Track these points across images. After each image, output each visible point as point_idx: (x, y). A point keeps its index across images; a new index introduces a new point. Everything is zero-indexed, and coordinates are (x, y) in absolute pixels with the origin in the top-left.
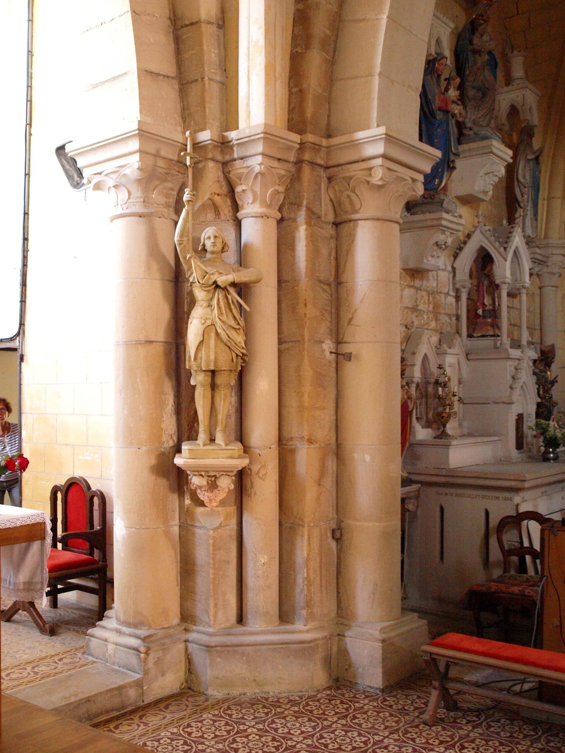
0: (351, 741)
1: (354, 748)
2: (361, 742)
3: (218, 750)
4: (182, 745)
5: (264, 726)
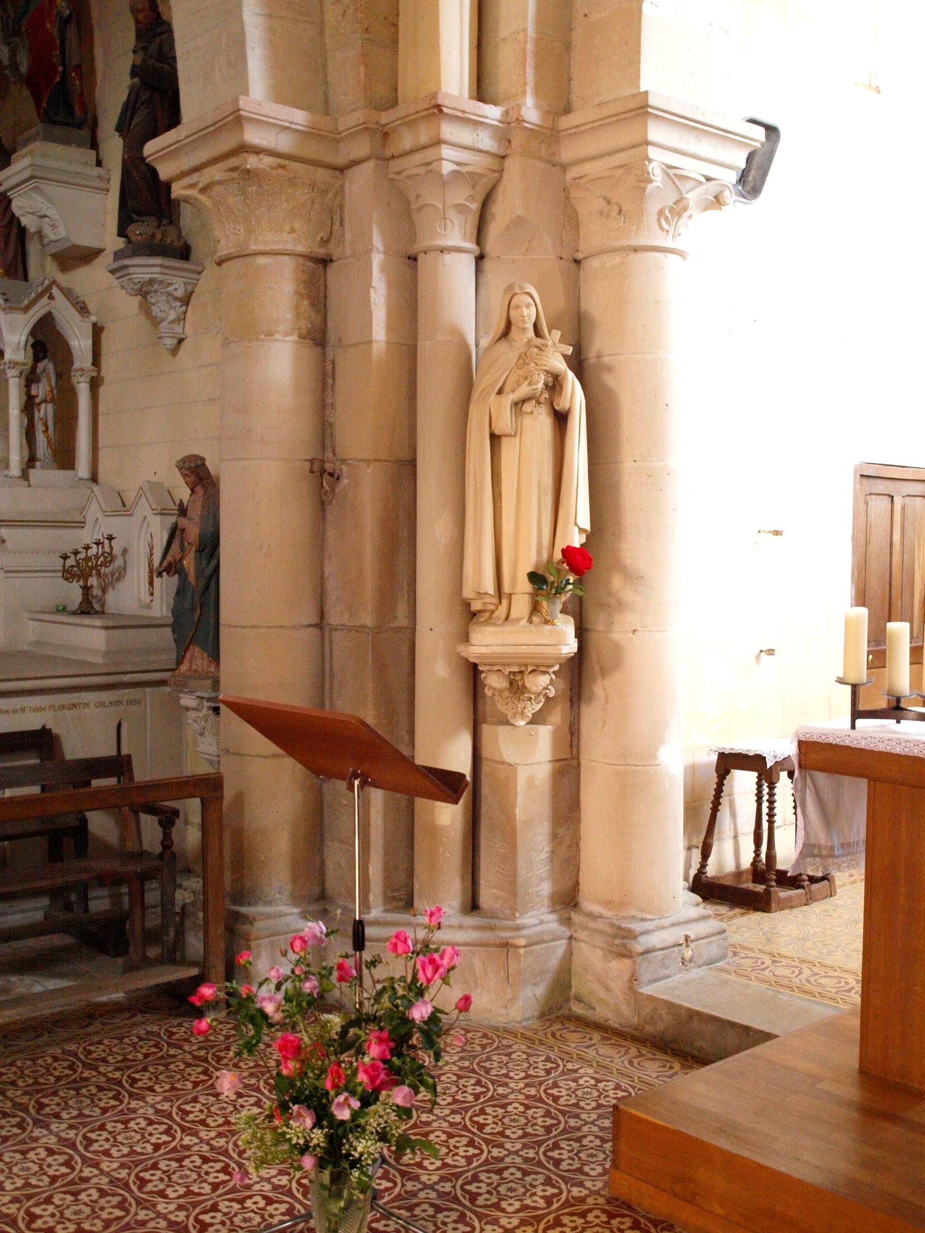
0: (62, 1213)
1: (108, 1223)
2: (41, 1217)
3: (171, 1224)
4: (487, 1125)
5: (566, 1122)
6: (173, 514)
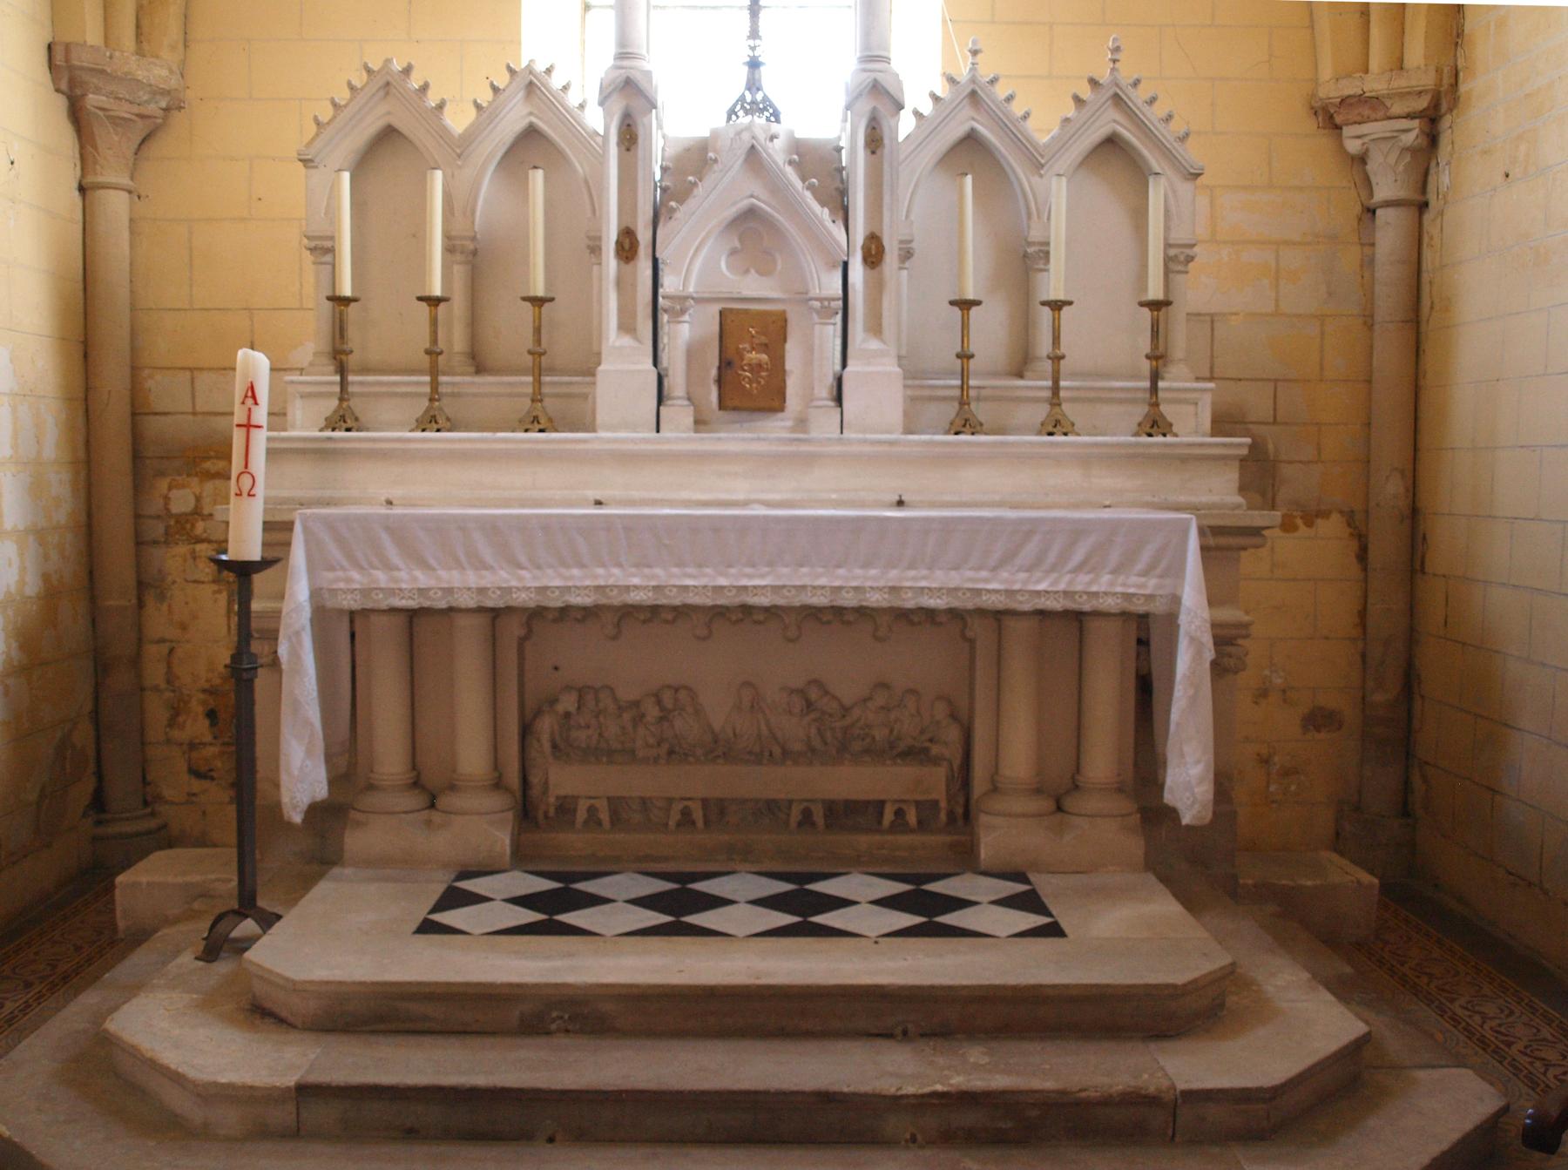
6: (1036, 400)
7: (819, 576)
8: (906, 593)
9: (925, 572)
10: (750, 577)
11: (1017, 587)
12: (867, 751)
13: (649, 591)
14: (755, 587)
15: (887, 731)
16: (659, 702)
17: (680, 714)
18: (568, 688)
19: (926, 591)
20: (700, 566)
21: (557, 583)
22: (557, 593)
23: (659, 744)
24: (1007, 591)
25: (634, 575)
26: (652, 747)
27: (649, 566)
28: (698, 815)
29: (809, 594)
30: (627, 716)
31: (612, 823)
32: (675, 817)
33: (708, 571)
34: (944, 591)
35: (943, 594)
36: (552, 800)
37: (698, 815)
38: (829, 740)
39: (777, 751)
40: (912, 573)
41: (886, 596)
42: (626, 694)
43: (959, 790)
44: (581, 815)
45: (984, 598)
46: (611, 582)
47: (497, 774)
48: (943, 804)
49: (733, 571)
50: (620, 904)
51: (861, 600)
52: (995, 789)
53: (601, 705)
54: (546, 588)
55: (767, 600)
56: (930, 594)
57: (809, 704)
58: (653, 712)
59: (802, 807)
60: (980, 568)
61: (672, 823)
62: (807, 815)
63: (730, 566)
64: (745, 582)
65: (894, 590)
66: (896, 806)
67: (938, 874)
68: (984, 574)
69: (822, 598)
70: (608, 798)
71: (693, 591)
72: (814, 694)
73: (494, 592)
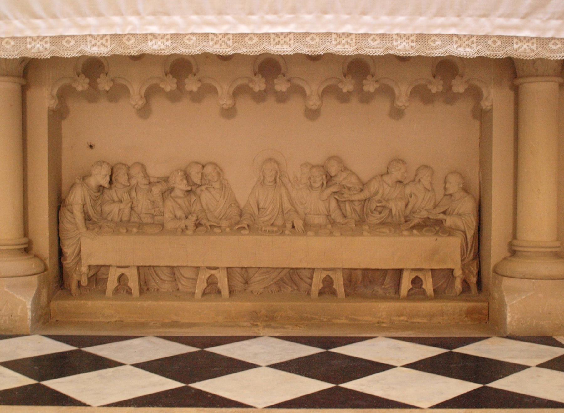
7: (345, 23)
8: (434, 41)
9: (454, 19)
10: (272, 24)
11: (549, 35)
12: (383, 224)
13: (167, 40)
14: (276, 35)
15: (402, 205)
16: (187, 176)
17: (207, 189)
18: (101, 162)
19: (455, 39)
20: (220, 13)
21: (73, 32)
22: (73, 43)
23: (187, 217)
24: (538, 39)
25: (151, 23)
26: (180, 219)
27: (167, 14)
28: (223, 284)
29: (334, 42)
30: (156, 190)
31: (141, 291)
32: (201, 286)
33: (229, 18)
34: (474, 39)
35: (473, 43)
36: (84, 269)
37: (223, 284)
38: (348, 213)
39: (299, 224)
40: (440, 20)
41: (414, 44)
42: (155, 172)
43: (473, 260)
44: (112, 284)
45: (515, 46)
46: (128, 30)
47: (25, 240)
48: (458, 273)
49: (254, 18)
50: (128, 368)
51: (387, 49)
52: (513, 252)
53: (133, 182)
54: (62, 37)
55: (290, 49)
56: (460, 42)
57: (329, 178)
58: (181, 186)
59: (324, 276)
60: (508, 16)
61: (198, 291)
62: (328, 283)
63: (251, 13)
64: (266, 29)
65: (422, 37)
66: (413, 275)
67: (478, 338)
68: (515, 21)
69: (347, 46)
70: (138, 267)
71: (213, 40)
72: (333, 169)
73: (8, 43)
